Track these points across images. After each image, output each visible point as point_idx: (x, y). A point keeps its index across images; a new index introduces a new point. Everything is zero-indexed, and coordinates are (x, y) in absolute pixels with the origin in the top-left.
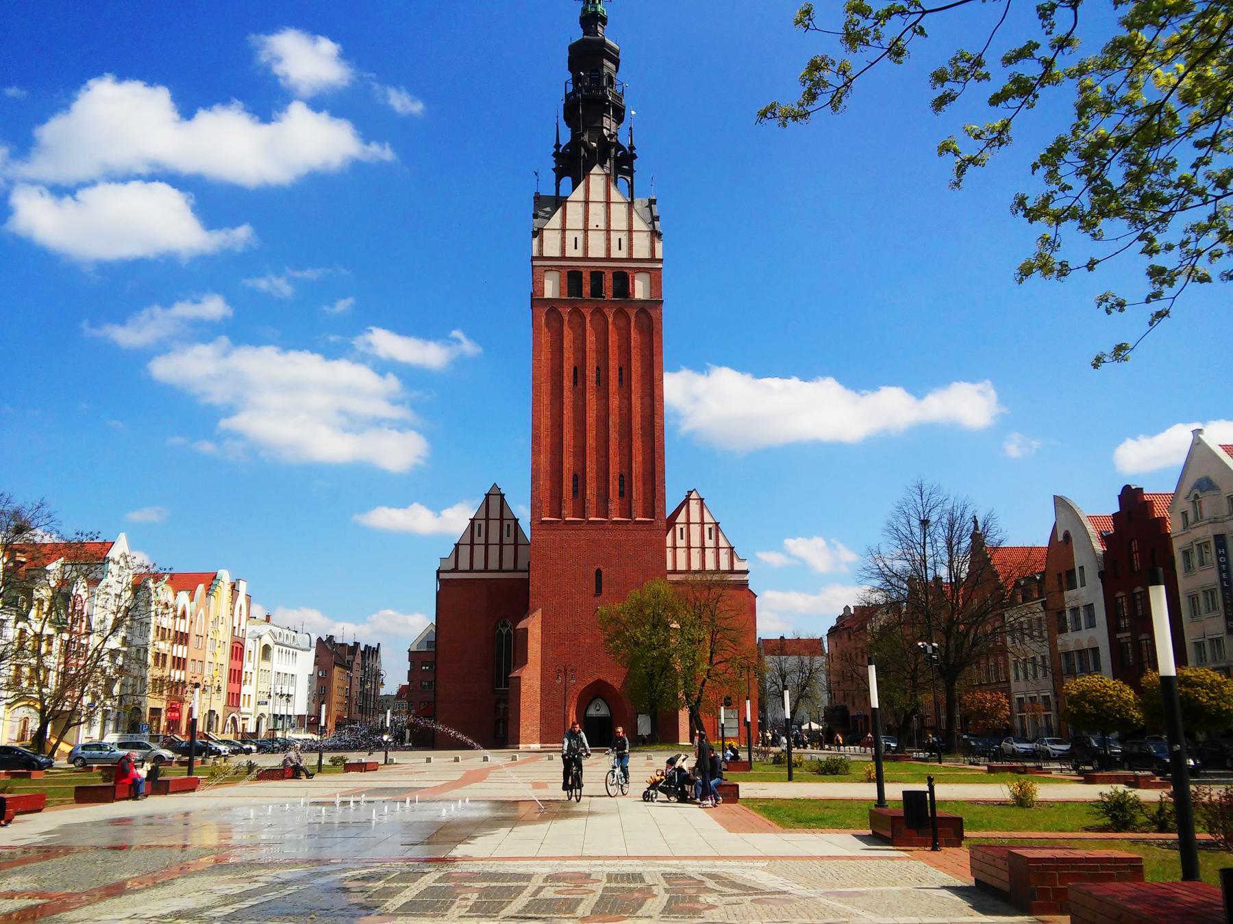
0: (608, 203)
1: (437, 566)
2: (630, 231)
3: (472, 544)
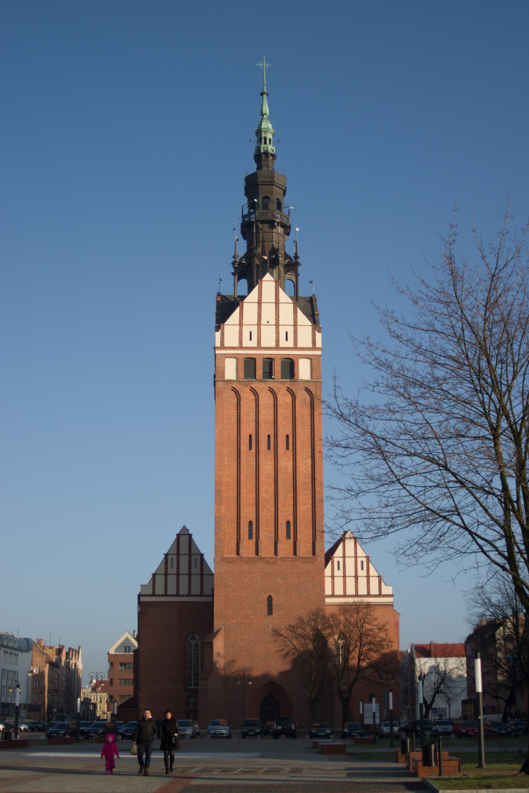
0: (277, 303)
1: (138, 591)
2: (295, 325)
3: (166, 574)
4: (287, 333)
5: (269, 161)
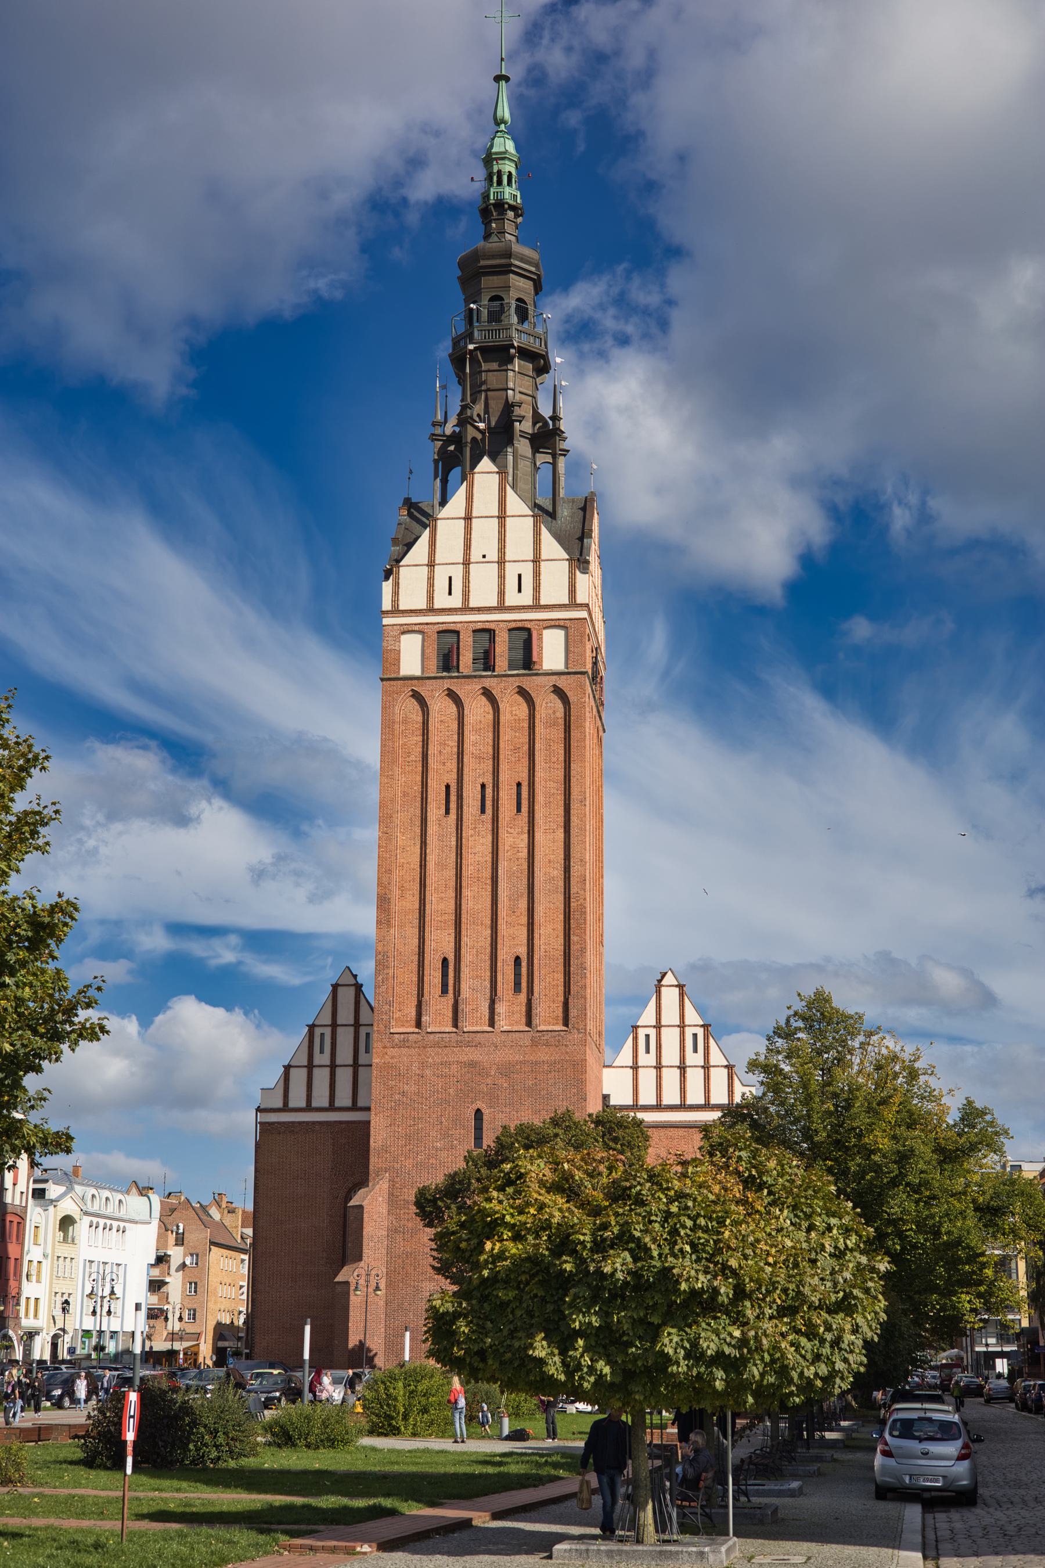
2: (536, 561)
3: (310, 1067)
4: (520, 576)
5: (506, 221)
